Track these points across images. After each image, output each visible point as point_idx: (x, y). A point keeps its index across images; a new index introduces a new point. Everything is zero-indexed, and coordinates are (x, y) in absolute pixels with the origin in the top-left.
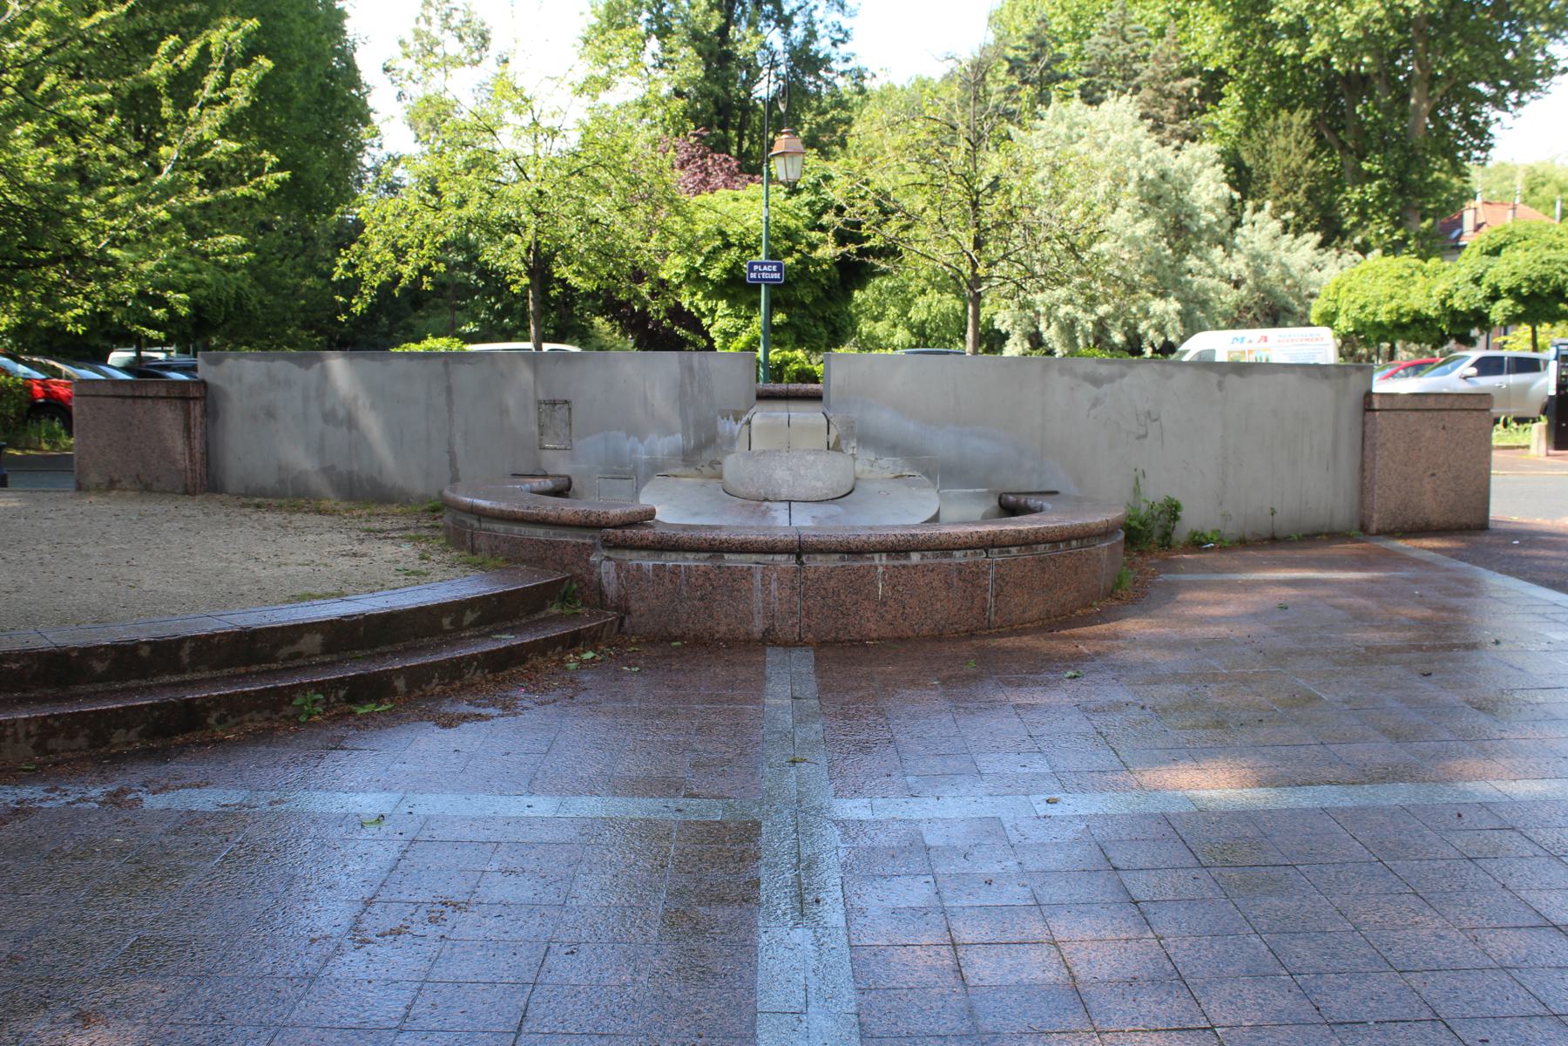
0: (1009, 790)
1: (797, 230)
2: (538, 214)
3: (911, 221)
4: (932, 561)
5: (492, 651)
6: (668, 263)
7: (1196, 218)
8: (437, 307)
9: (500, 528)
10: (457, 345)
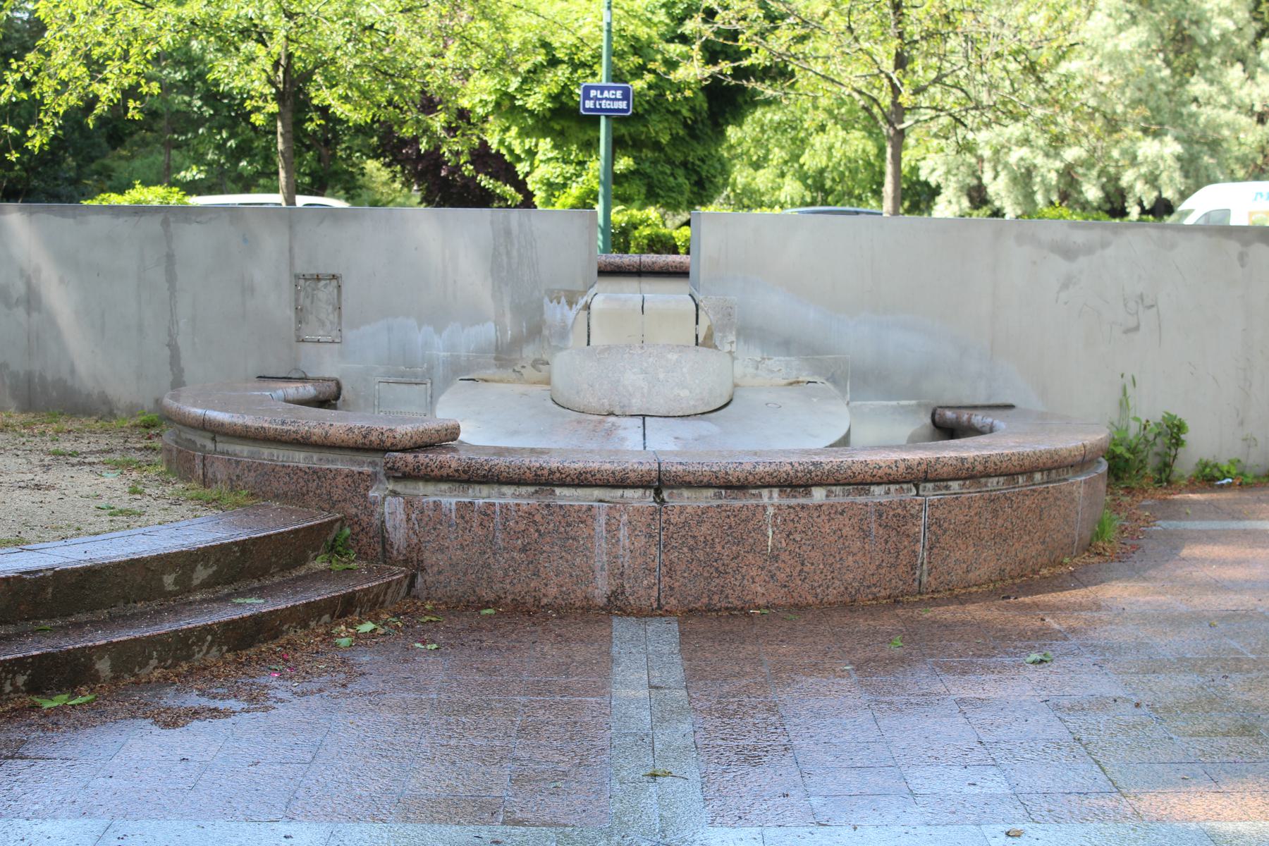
0: (954, 818)
1: (650, 43)
2: (290, 16)
3: (808, 29)
4: (842, 500)
5: (233, 621)
6: (470, 85)
7: (1206, 25)
8: (144, 143)
9: (243, 450)
10: (175, 197)
